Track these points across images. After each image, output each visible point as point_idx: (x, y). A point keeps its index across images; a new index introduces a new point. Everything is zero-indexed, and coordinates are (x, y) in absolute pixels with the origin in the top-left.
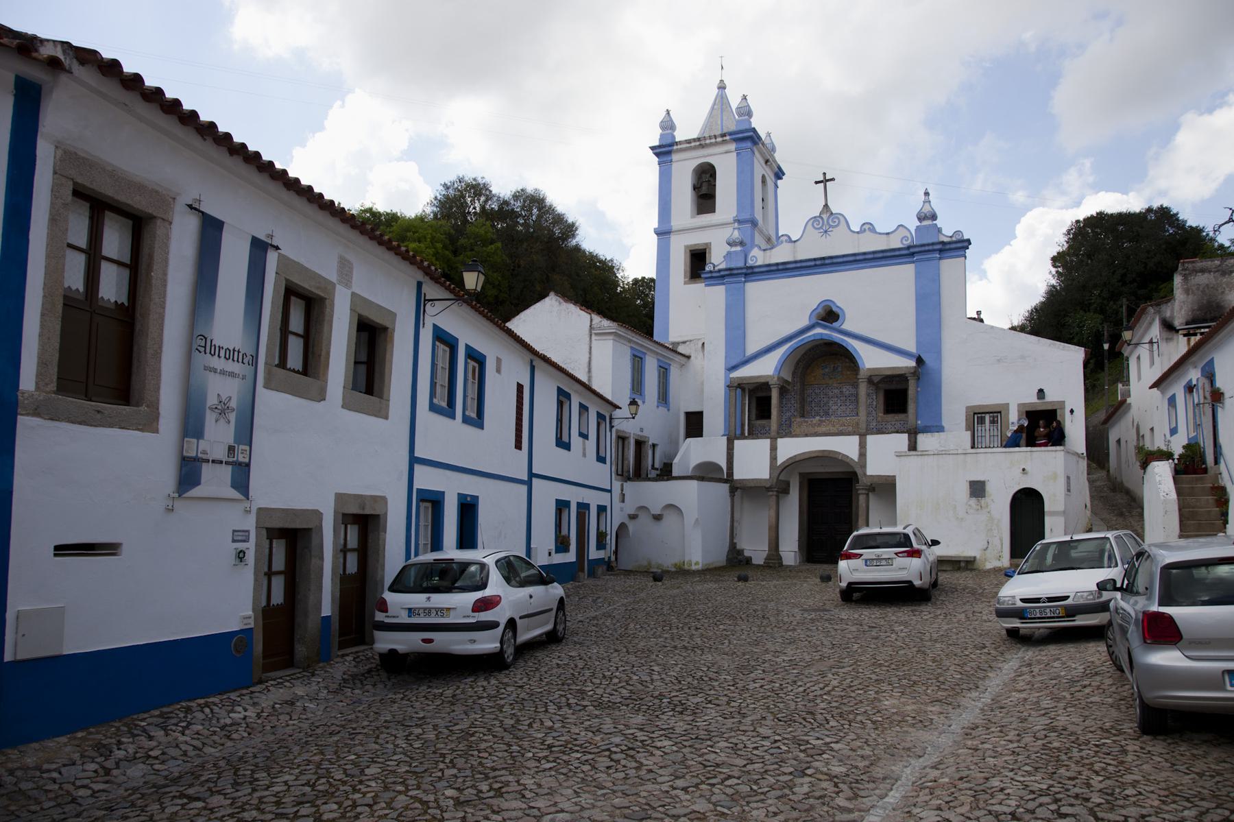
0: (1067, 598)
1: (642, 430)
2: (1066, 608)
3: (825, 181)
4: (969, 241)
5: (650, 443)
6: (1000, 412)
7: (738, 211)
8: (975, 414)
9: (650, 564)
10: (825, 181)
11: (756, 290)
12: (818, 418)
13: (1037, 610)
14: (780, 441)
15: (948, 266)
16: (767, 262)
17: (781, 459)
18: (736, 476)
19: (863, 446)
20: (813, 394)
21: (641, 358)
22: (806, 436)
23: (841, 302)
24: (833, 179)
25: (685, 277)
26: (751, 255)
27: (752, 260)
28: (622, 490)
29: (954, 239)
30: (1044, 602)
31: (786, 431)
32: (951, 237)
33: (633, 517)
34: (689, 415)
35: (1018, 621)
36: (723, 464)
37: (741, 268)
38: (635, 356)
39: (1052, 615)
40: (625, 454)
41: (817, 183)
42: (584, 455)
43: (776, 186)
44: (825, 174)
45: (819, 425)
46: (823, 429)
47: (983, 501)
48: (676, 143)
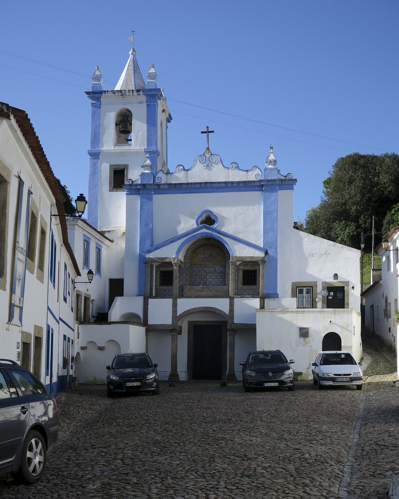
0: (350, 374)
1: (87, 290)
2: (351, 378)
3: (208, 132)
4: (295, 180)
5: (91, 299)
6: (312, 287)
7: (148, 146)
8: (297, 287)
9: (95, 379)
10: (208, 132)
11: (159, 199)
12: (201, 286)
13: (340, 378)
14: (179, 300)
15: (282, 194)
16: (168, 182)
17: (179, 312)
18: (150, 322)
19: (232, 305)
20: (197, 270)
21: (88, 242)
22: (196, 297)
23: (216, 210)
24: (212, 132)
25: (110, 186)
26: (157, 177)
27: (158, 180)
28: (78, 330)
29: (287, 178)
30: (342, 376)
31: (182, 295)
32: (285, 177)
33: (83, 348)
34: (112, 281)
35: (332, 382)
36: (140, 313)
37: (151, 184)
38: (85, 240)
39: (346, 380)
40: (79, 306)
41: (202, 132)
42: (69, 307)
43: (167, 127)
44: (208, 127)
45: (202, 291)
46: (204, 293)
47: (307, 339)
48: (105, 91)
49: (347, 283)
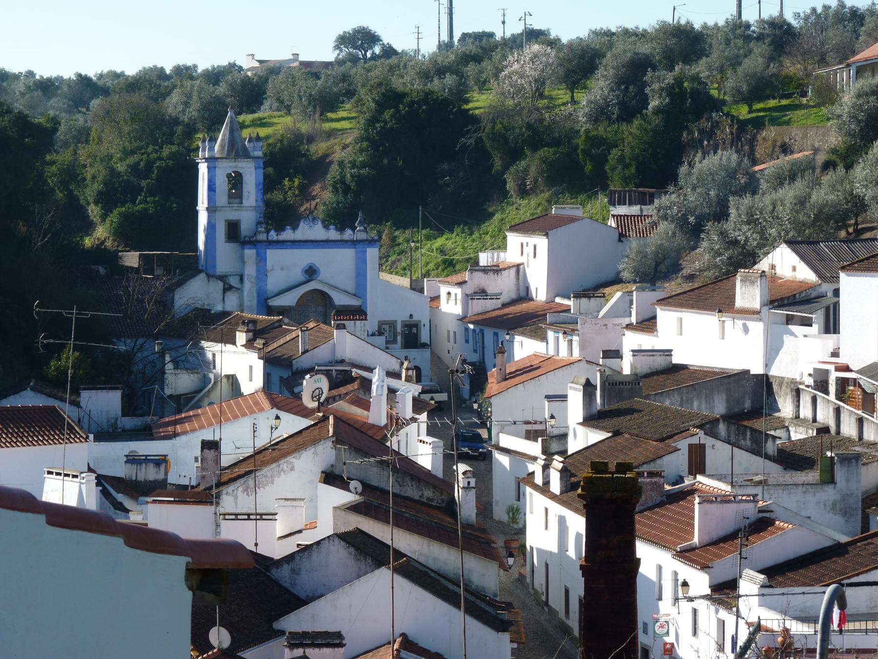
49: (420, 321)
